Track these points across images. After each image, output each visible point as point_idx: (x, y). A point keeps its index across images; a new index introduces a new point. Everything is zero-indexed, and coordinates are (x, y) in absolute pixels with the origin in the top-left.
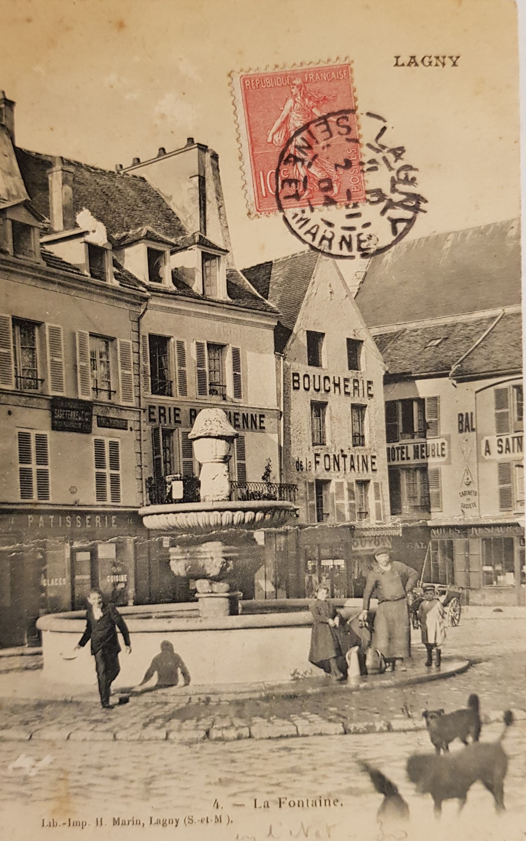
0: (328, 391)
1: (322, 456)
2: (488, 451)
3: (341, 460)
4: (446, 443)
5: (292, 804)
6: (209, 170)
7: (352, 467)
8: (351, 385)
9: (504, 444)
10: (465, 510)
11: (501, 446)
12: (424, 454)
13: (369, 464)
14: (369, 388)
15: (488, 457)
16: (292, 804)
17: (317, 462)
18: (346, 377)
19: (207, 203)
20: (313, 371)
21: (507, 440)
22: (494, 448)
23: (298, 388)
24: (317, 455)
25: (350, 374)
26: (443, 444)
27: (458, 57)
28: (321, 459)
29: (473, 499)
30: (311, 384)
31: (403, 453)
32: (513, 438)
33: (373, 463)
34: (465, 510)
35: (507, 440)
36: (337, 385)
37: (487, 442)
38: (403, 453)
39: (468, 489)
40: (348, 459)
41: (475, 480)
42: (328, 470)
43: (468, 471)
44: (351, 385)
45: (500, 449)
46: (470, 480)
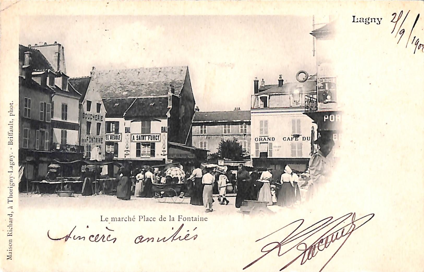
0: (91, 119)
1: (89, 138)
2: (134, 139)
3: (94, 139)
4: (121, 135)
5: (185, 219)
6: (61, 51)
7: (96, 142)
8: (97, 117)
9: (139, 137)
10: (126, 156)
11: (138, 138)
12: (114, 138)
13: (101, 141)
14: (102, 119)
15: (133, 141)
16: (185, 219)
17: (88, 140)
18: (96, 115)
19: (60, 61)
20: (88, 112)
21: (140, 136)
22: (135, 138)
23: (84, 118)
24: (88, 138)
25: (97, 114)
26: (120, 136)
27: (381, 19)
28: (88, 139)
29: (128, 153)
30: (87, 116)
31: (107, 137)
32: (141, 136)
33: (102, 141)
34: (126, 156)
35: (140, 136)
36: (94, 117)
37: (134, 136)
38: (107, 137)
39: (127, 150)
40: (95, 139)
41: (129, 147)
42: (90, 142)
43: (127, 145)
44: (97, 117)
45: (137, 139)
46: (128, 147)
